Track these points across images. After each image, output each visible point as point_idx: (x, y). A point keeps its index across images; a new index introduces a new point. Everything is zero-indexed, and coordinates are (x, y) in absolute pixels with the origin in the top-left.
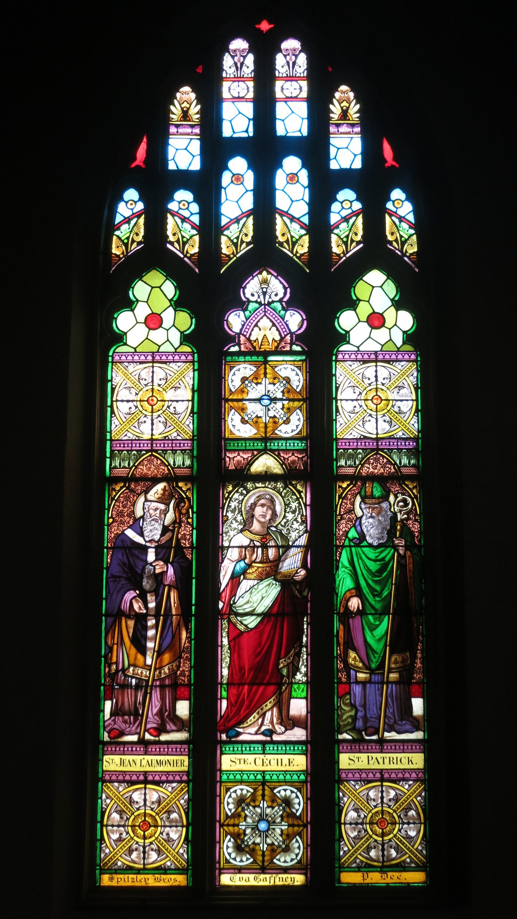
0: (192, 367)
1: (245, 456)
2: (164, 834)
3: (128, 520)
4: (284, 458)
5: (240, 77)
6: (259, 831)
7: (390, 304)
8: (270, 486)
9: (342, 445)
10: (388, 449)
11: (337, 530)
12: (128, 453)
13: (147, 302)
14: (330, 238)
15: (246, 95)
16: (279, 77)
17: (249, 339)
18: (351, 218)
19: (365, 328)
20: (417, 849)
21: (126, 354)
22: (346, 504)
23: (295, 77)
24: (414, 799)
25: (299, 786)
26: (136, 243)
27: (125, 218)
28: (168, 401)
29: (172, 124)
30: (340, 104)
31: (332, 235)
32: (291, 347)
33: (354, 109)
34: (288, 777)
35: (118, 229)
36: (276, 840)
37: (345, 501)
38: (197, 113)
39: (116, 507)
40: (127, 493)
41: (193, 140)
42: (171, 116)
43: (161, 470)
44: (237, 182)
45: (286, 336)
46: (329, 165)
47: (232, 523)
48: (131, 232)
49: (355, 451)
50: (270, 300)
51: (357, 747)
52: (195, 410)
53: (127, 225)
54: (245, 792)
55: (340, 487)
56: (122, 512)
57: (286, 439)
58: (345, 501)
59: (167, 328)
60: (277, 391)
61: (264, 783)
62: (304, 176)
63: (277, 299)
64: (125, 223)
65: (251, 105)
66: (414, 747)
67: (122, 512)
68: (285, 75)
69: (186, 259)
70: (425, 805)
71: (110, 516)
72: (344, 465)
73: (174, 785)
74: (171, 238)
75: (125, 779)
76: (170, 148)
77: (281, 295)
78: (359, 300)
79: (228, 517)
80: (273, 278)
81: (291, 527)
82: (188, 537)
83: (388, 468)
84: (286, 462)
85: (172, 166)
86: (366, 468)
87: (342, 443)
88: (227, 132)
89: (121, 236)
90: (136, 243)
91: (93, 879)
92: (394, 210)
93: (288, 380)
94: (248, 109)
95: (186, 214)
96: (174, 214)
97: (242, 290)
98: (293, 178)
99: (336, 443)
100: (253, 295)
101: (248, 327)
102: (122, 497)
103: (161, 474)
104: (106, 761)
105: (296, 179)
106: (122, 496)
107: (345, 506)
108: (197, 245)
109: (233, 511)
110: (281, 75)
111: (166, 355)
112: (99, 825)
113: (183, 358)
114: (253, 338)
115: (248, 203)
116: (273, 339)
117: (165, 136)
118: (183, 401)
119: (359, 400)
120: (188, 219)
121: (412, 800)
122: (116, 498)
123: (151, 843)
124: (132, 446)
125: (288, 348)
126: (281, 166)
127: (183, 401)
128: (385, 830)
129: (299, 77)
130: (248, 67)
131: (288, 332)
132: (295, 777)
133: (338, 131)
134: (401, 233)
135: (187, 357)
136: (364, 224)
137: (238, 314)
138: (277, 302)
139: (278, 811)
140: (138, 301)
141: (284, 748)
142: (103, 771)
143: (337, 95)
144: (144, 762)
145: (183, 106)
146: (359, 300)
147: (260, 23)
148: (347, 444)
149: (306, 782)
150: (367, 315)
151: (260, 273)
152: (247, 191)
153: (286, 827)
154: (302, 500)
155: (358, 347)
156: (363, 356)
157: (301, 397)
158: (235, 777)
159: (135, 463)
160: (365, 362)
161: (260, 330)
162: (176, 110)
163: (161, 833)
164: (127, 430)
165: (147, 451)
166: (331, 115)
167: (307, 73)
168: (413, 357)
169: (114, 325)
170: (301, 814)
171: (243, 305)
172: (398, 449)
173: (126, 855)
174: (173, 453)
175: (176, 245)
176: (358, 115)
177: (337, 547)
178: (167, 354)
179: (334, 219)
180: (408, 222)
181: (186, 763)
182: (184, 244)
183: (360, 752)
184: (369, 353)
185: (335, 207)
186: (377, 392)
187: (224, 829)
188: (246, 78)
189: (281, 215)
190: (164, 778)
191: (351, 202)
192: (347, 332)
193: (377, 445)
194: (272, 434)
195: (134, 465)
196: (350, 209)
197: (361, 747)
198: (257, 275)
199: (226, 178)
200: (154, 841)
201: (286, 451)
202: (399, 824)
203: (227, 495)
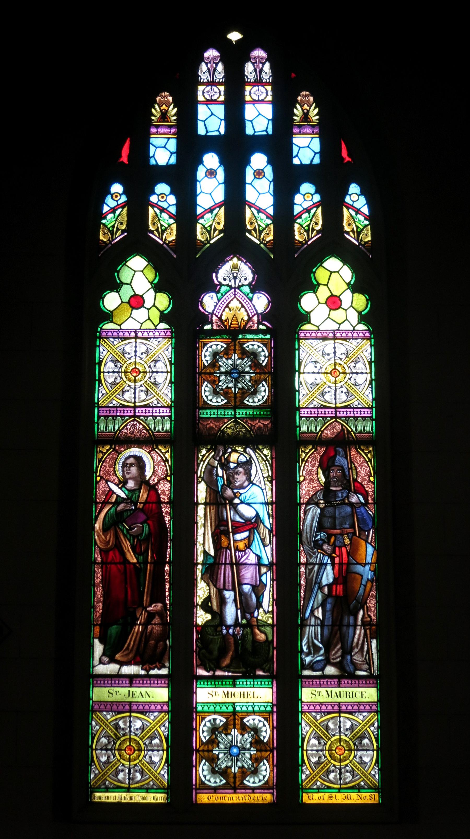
0: (369, 343)
9: (103, 413)
10: (144, 417)
11: (97, 490)
12: (315, 419)
14: (196, 226)
15: (265, 98)
16: (247, 82)
17: (220, 319)
18: (312, 209)
19: (325, 309)
22: (308, 466)
24: (368, 729)
25: (267, 716)
26: (120, 231)
27: (111, 208)
28: (321, 373)
29: (295, 125)
31: (198, 224)
33: (314, 112)
34: (218, 708)
35: (105, 218)
38: (174, 115)
39: (103, 467)
41: (171, 139)
42: (295, 118)
43: (143, 434)
44: (259, 176)
45: (253, 316)
46: (149, 161)
50: (240, 284)
52: (173, 380)
55: (101, 452)
61: (234, 713)
62: (269, 171)
63: (246, 283)
64: (110, 213)
65: (222, 107)
66: (329, 683)
72: (161, 430)
73: (365, 714)
76: (294, 147)
78: (319, 284)
80: (243, 264)
84: (253, 428)
87: (103, 411)
89: (106, 225)
90: (120, 231)
91: (297, 797)
94: (220, 110)
95: (164, 205)
96: (349, 207)
98: (259, 174)
101: (220, 308)
105: (263, 174)
112: (300, 749)
113: (361, 335)
114: (224, 318)
115: (220, 196)
116: (242, 319)
118: (309, 373)
119: (120, 372)
120: (166, 209)
121: (366, 729)
122: (305, 460)
124: (318, 413)
125: (255, 327)
126: (201, 162)
127: (309, 373)
129: (218, 82)
131: (255, 313)
132: (224, 708)
134: (259, 223)
135: (166, 334)
137: (211, 296)
138: (246, 285)
140: (319, 284)
141: (149, 682)
145: (162, 108)
146: (122, 283)
149: (272, 712)
150: (129, 297)
151: (232, 259)
153: (255, 752)
154: (269, 461)
158: (144, 707)
159: (321, 429)
161: (230, 310)
162: (156, 112)
163: (145, 756)
165: (332, 418)
166: (295, 118)
172: (354, 417)
176: (317, 117)
177: (272, 503)
178: (347, 331)
179: (297, 209)
184: (129, 331)
185: (298, 199)
187: (200, 754)
192: (309, 313)
193: (135, 412)
195: (320, 430)
196: (311, 201)
199: (201, 172)
200: (138, 763)
202: (144, 750)
203: (201, 457)
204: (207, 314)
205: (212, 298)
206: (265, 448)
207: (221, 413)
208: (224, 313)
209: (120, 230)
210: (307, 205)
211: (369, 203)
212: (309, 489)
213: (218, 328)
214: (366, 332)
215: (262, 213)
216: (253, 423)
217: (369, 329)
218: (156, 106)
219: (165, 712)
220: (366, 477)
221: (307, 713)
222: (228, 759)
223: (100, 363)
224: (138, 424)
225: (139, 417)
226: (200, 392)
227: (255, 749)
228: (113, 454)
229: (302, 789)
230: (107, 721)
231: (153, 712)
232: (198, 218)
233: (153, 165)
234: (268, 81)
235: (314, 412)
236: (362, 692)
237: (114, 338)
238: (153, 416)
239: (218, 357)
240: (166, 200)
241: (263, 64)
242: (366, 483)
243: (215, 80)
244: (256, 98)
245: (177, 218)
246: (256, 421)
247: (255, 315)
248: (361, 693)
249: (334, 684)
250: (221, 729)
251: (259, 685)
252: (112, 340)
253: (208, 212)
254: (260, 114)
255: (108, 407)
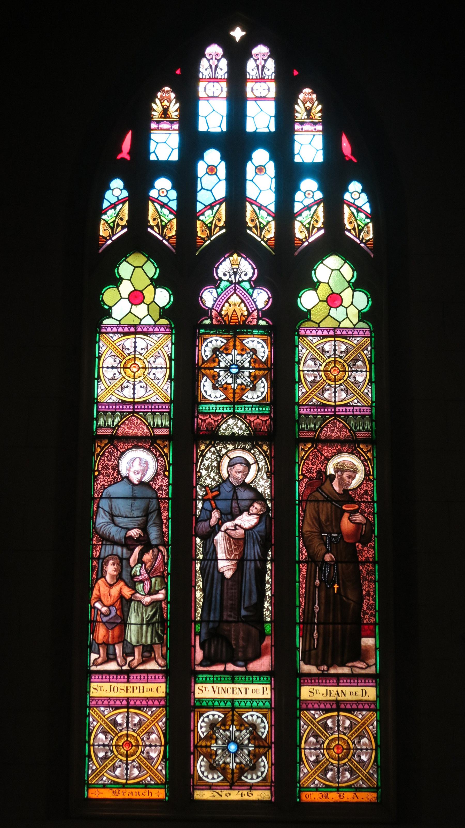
1: (216, 419)
2: (145, 752)
3: (113, 472)
4: (250, 421)
5: (215, 78)
6: (229, 752)
7: (149, 282)
8: (239, 447)
9: (102, 408)
10: (143, 412)
12: (112, 414)
13: (130, 280)
14: (293, 224)
16: (249, 79)
17: (220, 314)
20: (368, 773)
21: (111, 326)
22: (308, 464)
23: (217, 78)
26: (120, 227)
27: (111, 204)
30: (304, 104)
31: (296, 222)
32: (257, 322)
35: (105, 213)
36: (244, 759)
37: (103, 458)
39: (101, 461)
40: (315, 452)
44: (260, 173)
45: (253, 311)
46: (293, 158)
47: (206, 479)
48: (116, 217)
49: (145, 414)
50: (240, 279)
51: (317, 681)
53: (113, 210)
54: (216, 717)
56: (311, 469)
57: (253, 404)
58: (103, 458)
59: (346, 306)
60: (246, 361)
62: (271, 168)
63: (246, 278)
64: (111, 209)
66: (223, 679)
67: (107, 466)
68: (208, 77)
69: (262, 242)
70: (166, 730)
71: (300, 473)
74: (152, 223)
75: (320, 707)
76: (152, 142)
77: (250, 275)
79: (201, 473)
80: (243, 259)
81: (258, 483)
82: (370, 493)
83: (344, 431)
85: (153, 157)
86: (324, 432)
87: (102, 406)
88: (202, 127)
90: (218, 228)
92: (352, 201)
93: (254, 351)
95: (165, 200)
96: (154, 201)
97: (215, 269)
98: (260, 169)
99: (97, 406)
100: (225, 275)
102: (311, 456)
103: (141, 432)
104: (94, 688)
106: (311, 454)
107: (103, 462)
108: (175, 228)
109: (207, 469)
110: (251, 77)
111: (346, 330)
112: (87, 745)
117: (148, 130)
120: (166, 205)
123: (133, 761)
124: (116, 408)
126: (202, 158)
128: (340, 755)
130: (221, 70)
131: (255, 308)
132: (222, 704)
133: (302, 129)
134: (359, 222)
136: (226, 211)
137: (211, 291)
139: (245, 734)
141: (146, 677)
142: (90, 697)
143: (301, 96)
144: (249, 691)
146: (319, 282)
147: (233, 29)
148: (107, 407)
150: (327, 296)
151: (232, 255)
152: (220, 180)
153: (253, 748)
154: (167, 459)
155: (120, 321)
156: (148, 329)
157: (266, 367)
158: (246, 704)
160: (125, 334)
161: (230, 305)
162: (157, 107)
163: (142, 752)
164: (112, 394)
167: (275, 76)
168: (368, 333)
169: (299, 304)
170: (266, 737)
171: (216, 283)
173: (110, 771)
174: (152, 414)
175: (156, 228)
179: (297, 207)
180: (365, 213)
181: (197, 691)
182: (262, 229)
183: (319, 685)
185: (298, 196)
186: (135, 361)
188: (220, 79)
189: (251, 204)
190: (354, 706)
191: (351, 193)
192: (110, 308)
193: (335, 411)
194: (239, 399)
195: (320, 427)
197: (320, 681)
198: (228, 257)
200: (135, 759)
201: (252, 415)
204: (207, 309)
205: (211, 293)
206: (264, 443)
207: (219, 408)
208: (224, 308)
209: (218, 226)
210: (308, 202)
211: (371, 200)
212: (104, 483)
213: (217, 323)
214: (131, 327)
215: (263, 210)
216: (252, 419)
217: (170, 324)
218: (157, 100)
219: (163, 706)
220: (161, 472)
221: (95, 708)
222: (227, 755)
223: (99, 358)
224: (338, 423)
225: (138, 413)
226: (198, 387)
227: (253, 745)
228: (111, 448)
229: (88, 784)
230: (104, 716)
231: (152, 707)
232: (198, 214)
233: (154, 161)
234: (270, 78)
235: (314, 409)
236: (233, 688)
237: (114, 333)
238: (152, 412)
239: (218, 353)
240: (166, 196)
241: (219, 60)
242: (160, 478)
243: (264, 77)
244: (258, 95)
245: (178, 214)
246: (219, 416)
247: (255, 310)
248: (232, 689)
249: (333, 682)
250: (218, 725)
251: (243, 682)
252: (111, 335)
253: (208, 209)
254: (214, 110)
255: (308, 405)
